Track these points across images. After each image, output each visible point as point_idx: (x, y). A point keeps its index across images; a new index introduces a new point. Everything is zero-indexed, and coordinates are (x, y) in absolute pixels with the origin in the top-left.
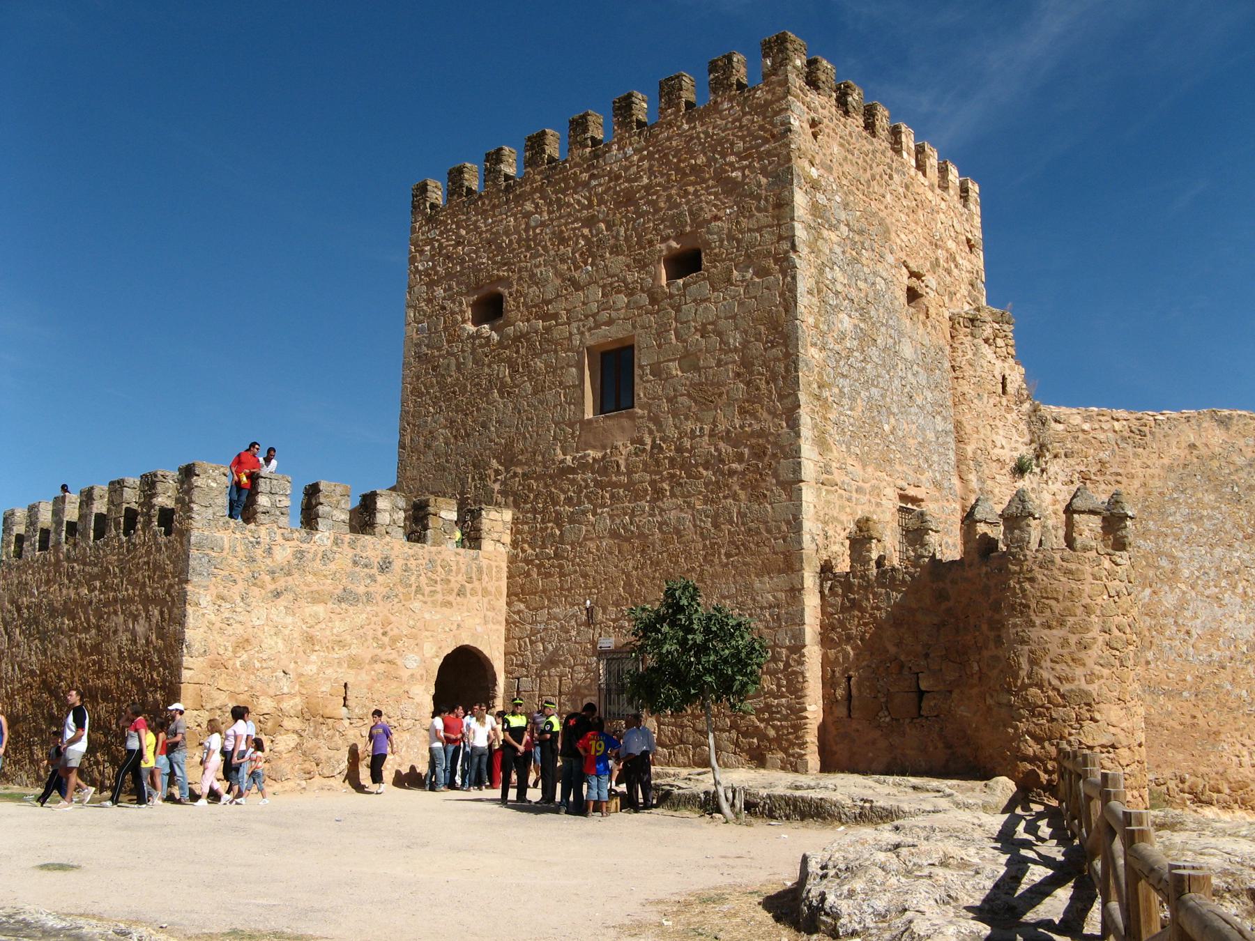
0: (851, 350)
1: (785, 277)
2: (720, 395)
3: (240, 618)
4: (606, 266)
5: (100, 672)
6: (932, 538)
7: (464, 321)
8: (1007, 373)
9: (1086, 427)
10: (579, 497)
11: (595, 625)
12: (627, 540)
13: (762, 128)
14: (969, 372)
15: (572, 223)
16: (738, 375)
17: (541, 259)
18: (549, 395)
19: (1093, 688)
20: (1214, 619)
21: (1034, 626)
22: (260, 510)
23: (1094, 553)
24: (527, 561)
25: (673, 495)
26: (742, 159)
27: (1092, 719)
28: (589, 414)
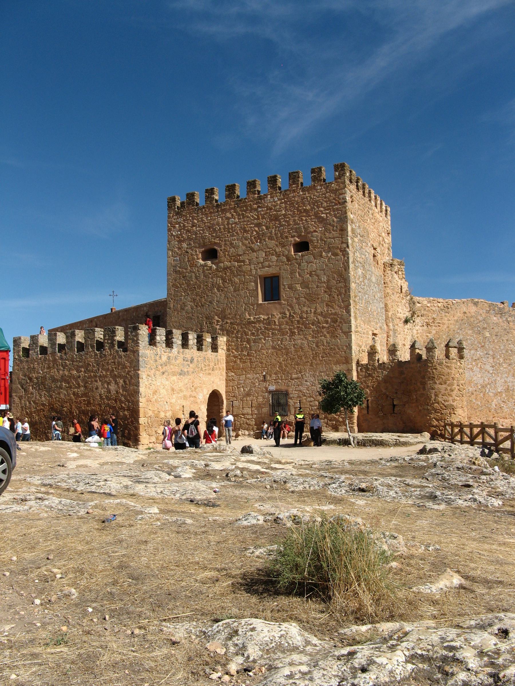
1: (344, 257)
2: (318, 299)
3: (154, 383)
4: (266, 244)
5: (89, 403)
6: (398, 353)
7: (198, 259)
8: (402, 284)
9: (429, 305)
10: (257, 333)
11: (266, 381)
12: (279, 350)
13: (334, 199)
14: (390, 285)
15: (250, 224)
16: (325, 292)
17: (236, 238)
18: (242, 293)
19: (454, 404)
20: (470, 377)
21: (436, 384)
22: (157, 342)
23: (455, 361)
24: (235, 357)
25: (299, 334)
26: (326, 210)
27: (454, 413)
28: (260, 302)
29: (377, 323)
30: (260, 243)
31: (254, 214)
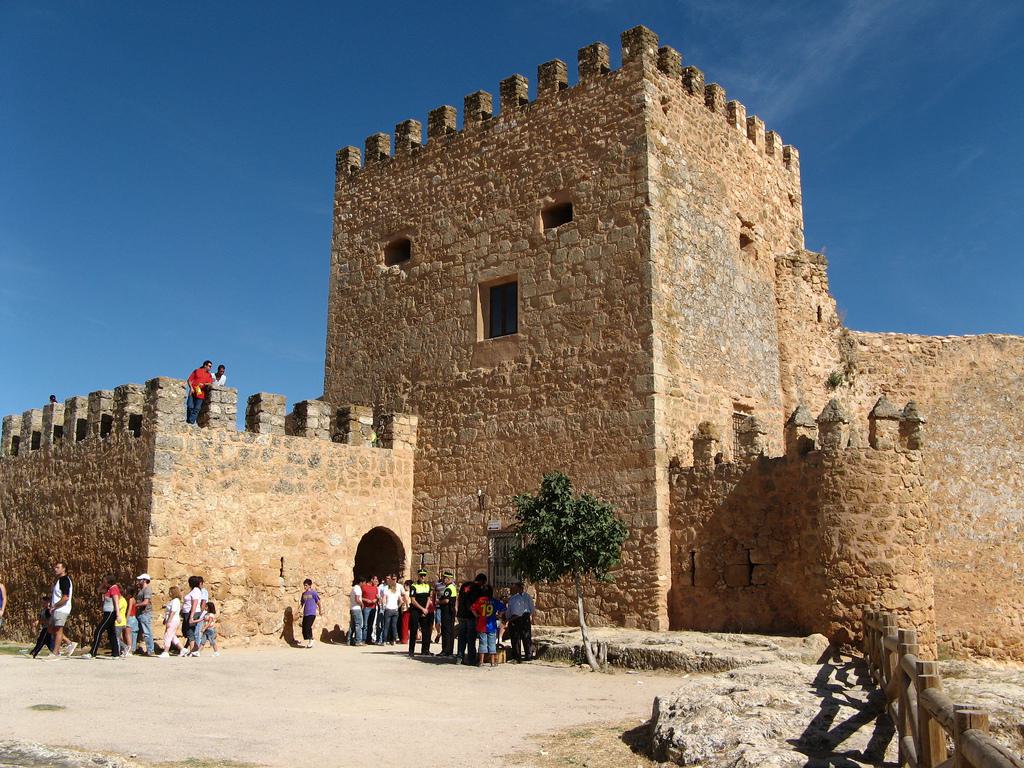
0: (694, 286)
2: (588, 322)
4: (494, 217)
6: (761, 439)
8: (822, 304)
9: (886, 348)
10: (472, 406)
11: (486, 510)
12: (512, 441)
14: (790, 303)
15: (467, 182)
18: (448, 323)
19: (892, 562)
22: (212, 416)
24: (430, 458)
26: (605, 129)
27: (891, 587)
28: (481, 338)
29: (749, 383)
30: (483, 216)
31: (474, 161)
